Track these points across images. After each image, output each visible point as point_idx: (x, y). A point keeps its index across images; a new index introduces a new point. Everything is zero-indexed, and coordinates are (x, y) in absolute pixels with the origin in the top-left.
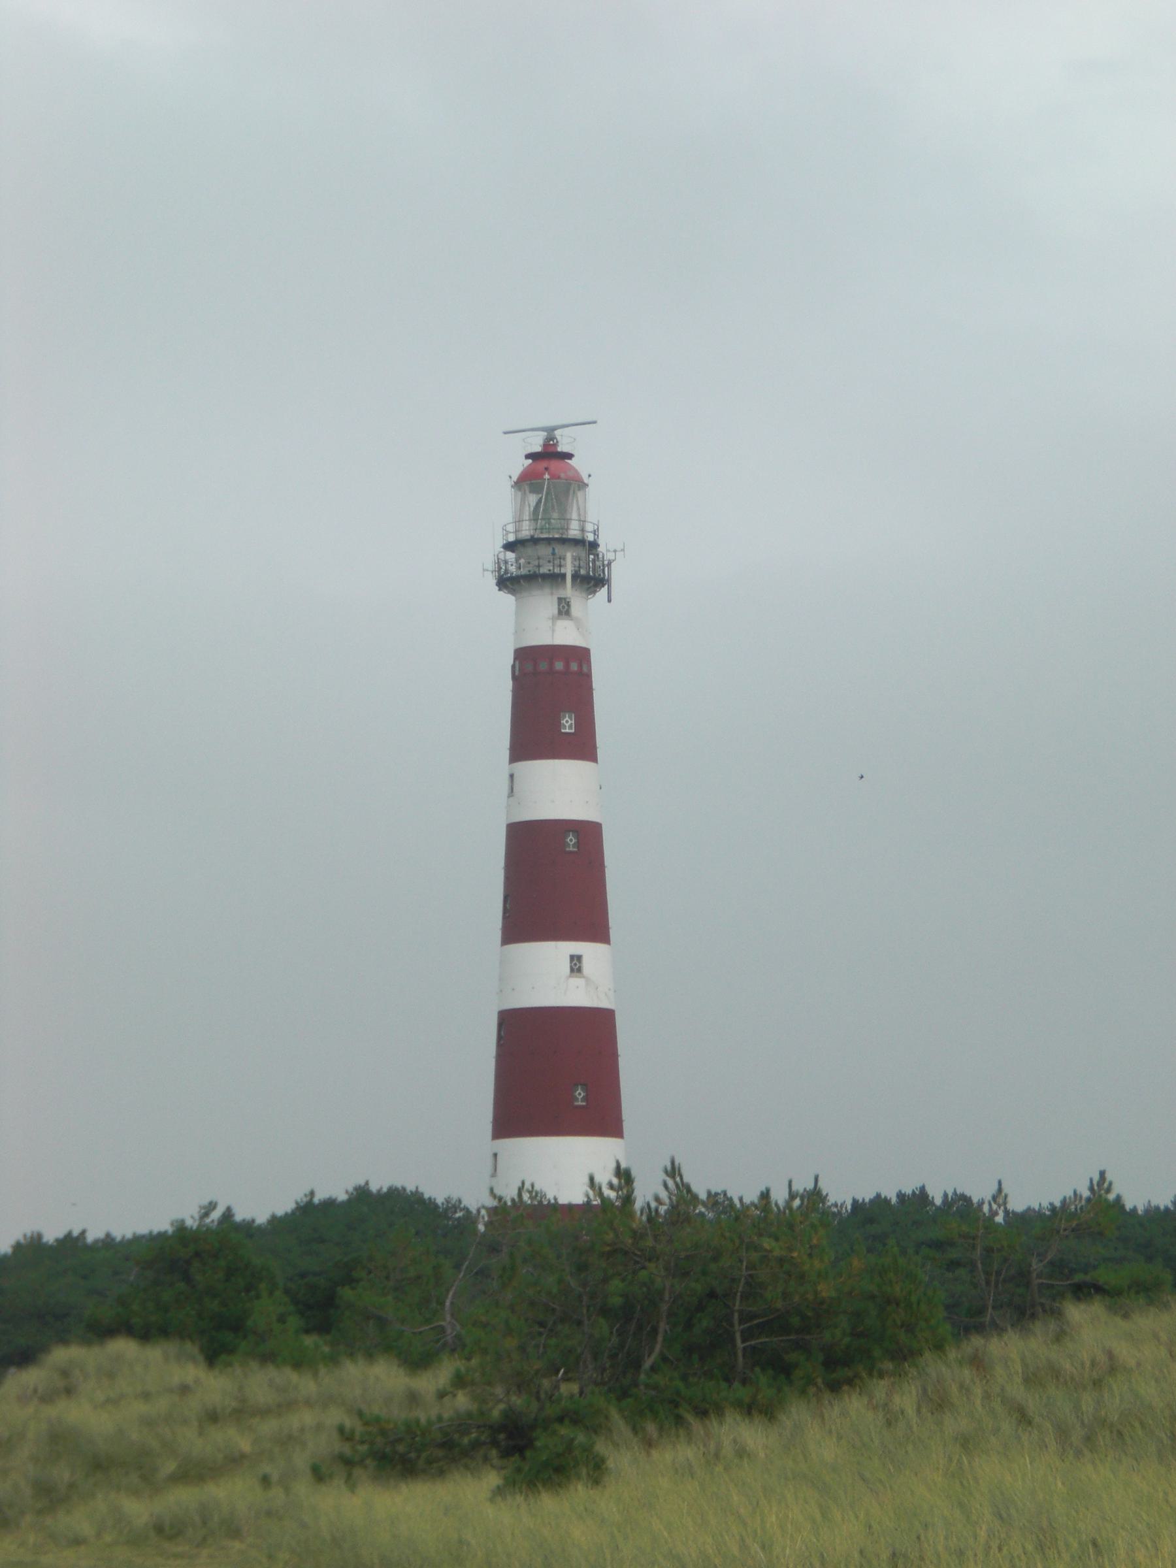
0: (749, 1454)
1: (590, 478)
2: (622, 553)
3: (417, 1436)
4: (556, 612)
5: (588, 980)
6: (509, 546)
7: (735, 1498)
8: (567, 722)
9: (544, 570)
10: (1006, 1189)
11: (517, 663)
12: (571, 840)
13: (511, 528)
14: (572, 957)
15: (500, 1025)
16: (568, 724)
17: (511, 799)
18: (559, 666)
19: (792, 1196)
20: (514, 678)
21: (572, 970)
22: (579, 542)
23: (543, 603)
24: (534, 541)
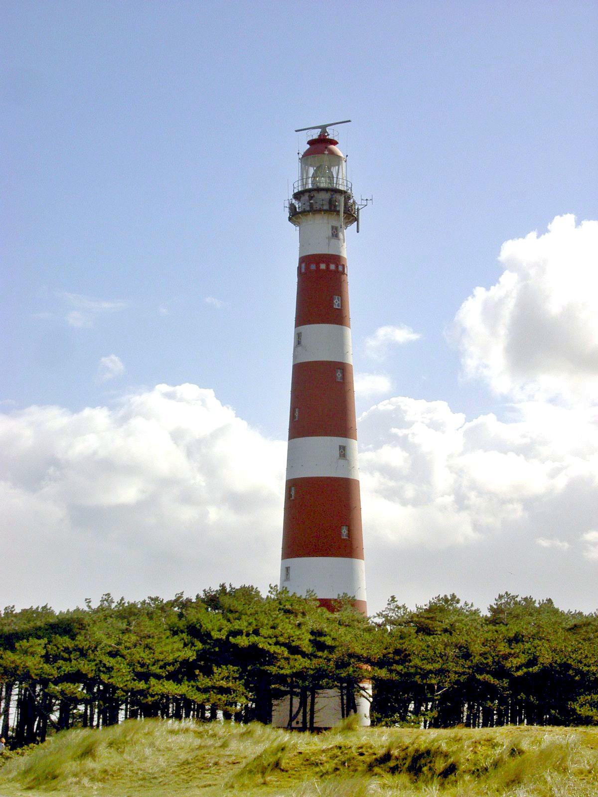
1: (298, 152)
2: (371, 201)
4: (331, 234)
6: (297, 196)
8: (336, 302)
10: (184, 593)
11: (303, 265)
14: (340, 447)
17: (300, 348)
18: (323, 266)
19: (50, 609)
21: (340, 456)
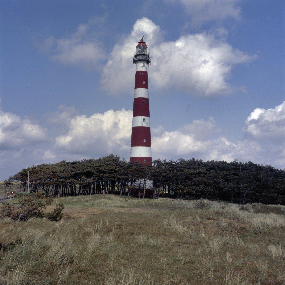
0: (208, 219)
3: (155, 186)
4: (142, 66)
5: (148, 90)
7: (203, 235)
9: (141, 59)
12: (144, 101)
13: (136, 53)
14: (144, 119)
15: (132, 129)
16: (144, 83)
20: (136, 76)
21: (144, 121)
22: (146, 55)
23: (140, 64)
24: (139, 55)
